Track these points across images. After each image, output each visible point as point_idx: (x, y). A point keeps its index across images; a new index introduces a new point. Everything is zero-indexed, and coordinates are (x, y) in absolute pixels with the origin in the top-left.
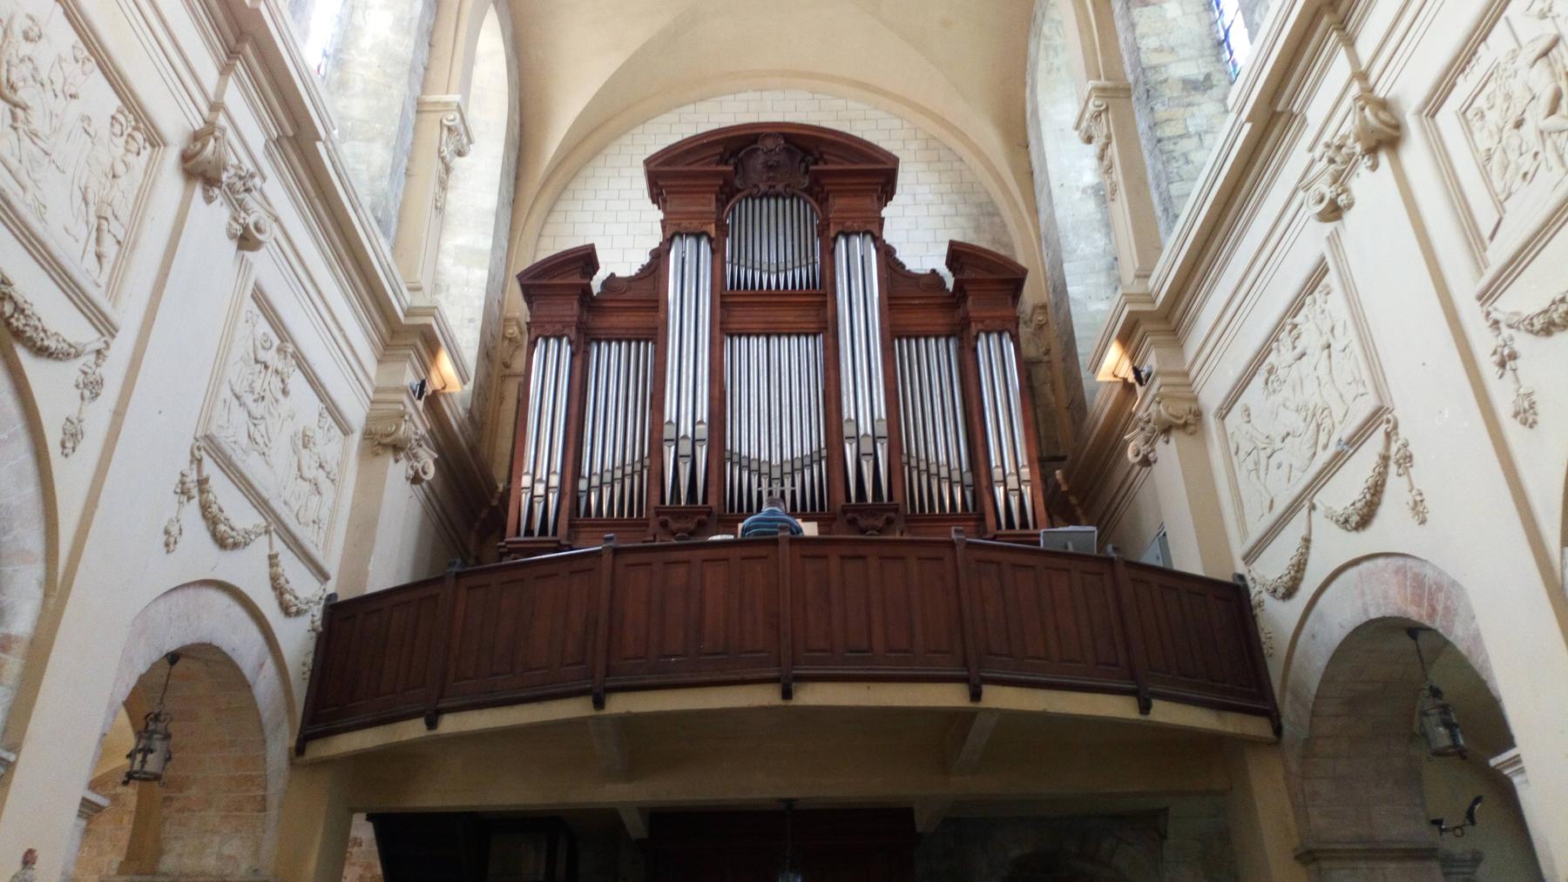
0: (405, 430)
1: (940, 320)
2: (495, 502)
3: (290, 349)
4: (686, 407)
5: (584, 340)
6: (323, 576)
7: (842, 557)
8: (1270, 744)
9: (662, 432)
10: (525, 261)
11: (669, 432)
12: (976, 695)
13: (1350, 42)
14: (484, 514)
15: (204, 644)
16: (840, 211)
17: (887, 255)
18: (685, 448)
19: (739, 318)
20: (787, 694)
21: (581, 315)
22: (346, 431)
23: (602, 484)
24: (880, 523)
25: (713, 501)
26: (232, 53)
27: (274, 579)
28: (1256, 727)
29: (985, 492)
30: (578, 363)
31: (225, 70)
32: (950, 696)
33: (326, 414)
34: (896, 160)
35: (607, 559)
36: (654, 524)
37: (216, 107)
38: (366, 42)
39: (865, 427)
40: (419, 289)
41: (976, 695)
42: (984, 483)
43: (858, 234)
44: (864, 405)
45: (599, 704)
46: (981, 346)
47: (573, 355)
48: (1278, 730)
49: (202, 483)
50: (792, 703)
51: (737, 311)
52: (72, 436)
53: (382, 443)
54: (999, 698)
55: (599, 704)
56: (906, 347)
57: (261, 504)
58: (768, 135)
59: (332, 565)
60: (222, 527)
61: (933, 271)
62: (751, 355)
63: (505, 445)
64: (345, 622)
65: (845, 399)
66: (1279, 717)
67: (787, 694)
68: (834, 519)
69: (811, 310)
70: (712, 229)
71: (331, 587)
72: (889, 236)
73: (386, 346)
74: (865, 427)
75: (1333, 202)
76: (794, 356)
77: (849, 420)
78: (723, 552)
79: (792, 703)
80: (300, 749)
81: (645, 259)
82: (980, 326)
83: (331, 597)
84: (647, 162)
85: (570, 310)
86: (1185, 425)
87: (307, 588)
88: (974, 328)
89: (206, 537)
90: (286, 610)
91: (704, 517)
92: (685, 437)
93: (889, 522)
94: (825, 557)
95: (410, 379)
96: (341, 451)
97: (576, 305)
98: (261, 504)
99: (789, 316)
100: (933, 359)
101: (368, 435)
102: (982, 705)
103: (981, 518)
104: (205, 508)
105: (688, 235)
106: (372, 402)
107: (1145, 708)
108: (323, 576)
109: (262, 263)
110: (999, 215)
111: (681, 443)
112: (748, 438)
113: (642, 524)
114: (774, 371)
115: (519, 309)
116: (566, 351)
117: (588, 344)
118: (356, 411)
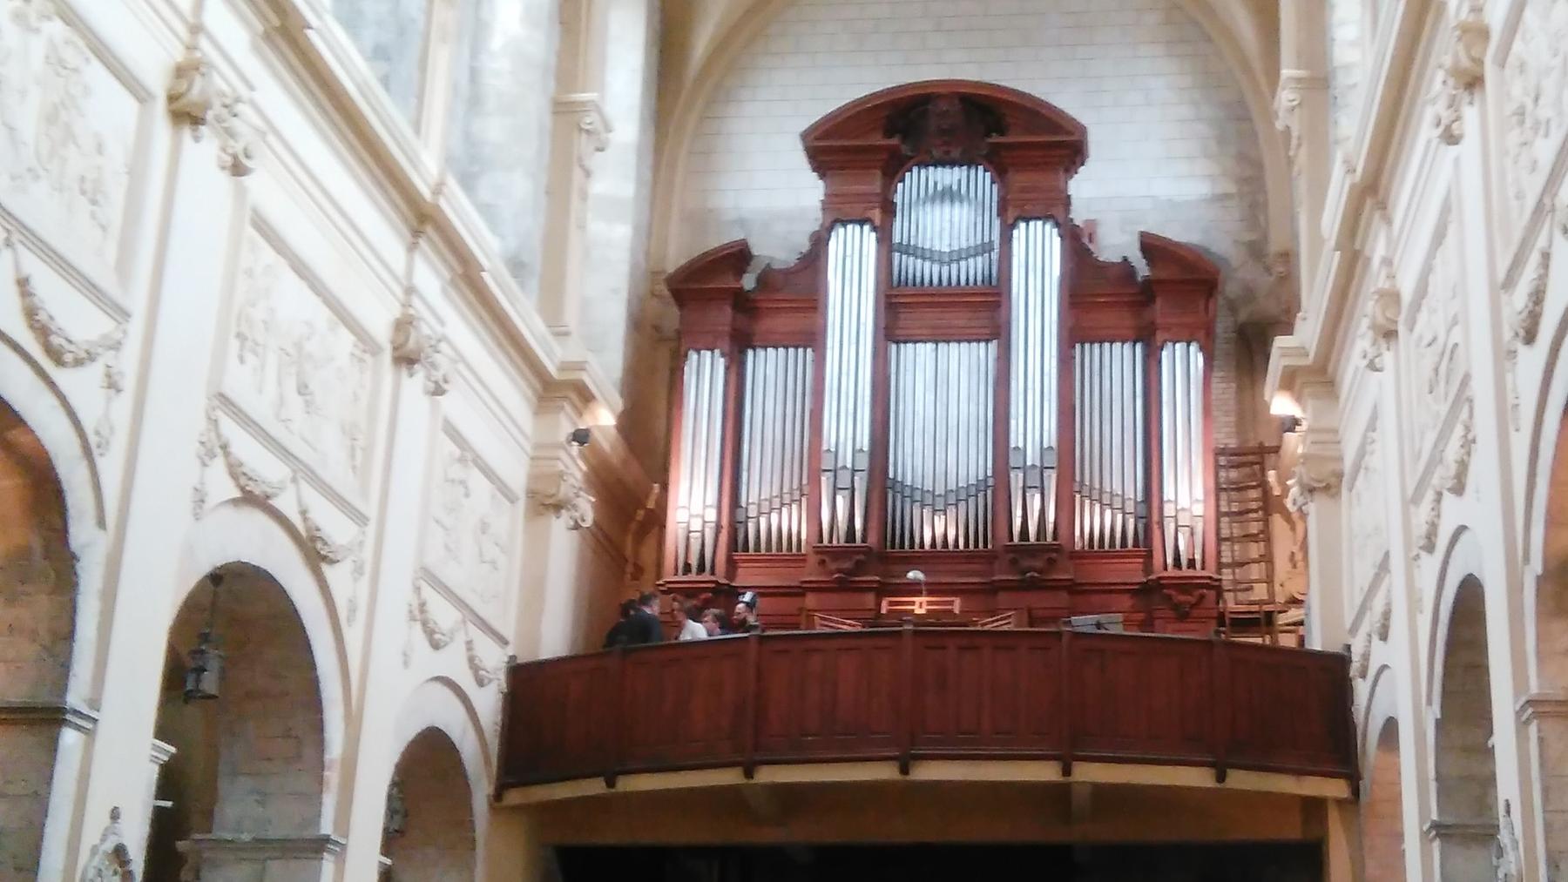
0: (565, 491)
1: (1126, 320)
2: (651, 505)
3: (469, 456)
4: (846, 431)
5: (739, 345)
6: (504, 642)
7: (961, 649)
8: (1351, 802)
9: (819, 460)
10: (676, 258)
11: (827, 463)
12: (1067, 771)
13: (1389, 221)
14: (641, 513)
15: (257, 569)
16: (1023, 190)
17: (1077, 244)
18: (844, 480)
19: (907, 320)
20: (905, 770)
21: (734, 319)
22: (512, 500)
23: (760, 514)
24: (1038, 564)
25: (873, 540)
26: (417, 233)
27: (471, 660)
28: (1334, 789)
29: (1155, 527)
30: (733, 378)
31: (412, 248)
32: (1045, 772)
33: (499, 495)
34: (1082, 130)
35: (753, 645)
36: (813, 560)
37: (410, 290)
38: (496, 42)
39: (1032, 458)
40: (566, 334)
41: (1067, 771)
42: (1155, 518)
43: (1039, 218)
44: (1035, 428)
45: (749, 774)
46: (1165, 355)
47: (727, 369)
48: (1356, 792)
49: (422, 605)
50: (908, 778)
51: (909, 310)
52: (353, 610)
53: (544, 504)
54: (1089, 773)
55: (749, 774)
56: (1091, 355)
57: (460, 603)
58: (940, 96)
59: (508, 632)
60: (437, 636)
61: (1125, 259)
62: (919, 362)
63: (661, 424)
64: (528, 685)
65: (1013, 422)
66: (1359, 778)
67: (905, 770)
68: (996, 557)
69: (979, 311)
70: (876, 215)
71: (510, 651)
72: (1079, 215)
73: (541, 399)
74: (1032, 458)
75: (1448, 128)
76: (965, 362)
77: (1017, 448)
78: (853, 643)
79: (908, 778)
80: (498, 796)
81: (805, 246)
82: (1166, 336)
83: (513, 658)
84: (805, 136)
85: (724, 316)
86: (1327, 488)
87: (495, 659)
88: (1159, 337)
89: (426, 644)
90: (481, 683)
91: (861, 557)
92: (845, 467)
93: (1051, 562)
94: (944, 648)
95: (566, 429)
96: (510, 520)
97: (728, 310)
98: (460, 603)
99: (960, 319)
100: (1118, 363)
101: (532, 494)
102: (1071, 779)
103: (1149, 556)
104: (425, 624)
105: (851, 222)
106: (532, 459)
107: (1221, 778)
108: (504, 642)
109: (451, 404)
110: (1250, 120)
111: (840, 472)
112: (914, 460)
113: (800, 559)
114: (942, 376)
115: (672, 316)
116: (721, 363)
117: (743, 353)
118: (517, 475)
